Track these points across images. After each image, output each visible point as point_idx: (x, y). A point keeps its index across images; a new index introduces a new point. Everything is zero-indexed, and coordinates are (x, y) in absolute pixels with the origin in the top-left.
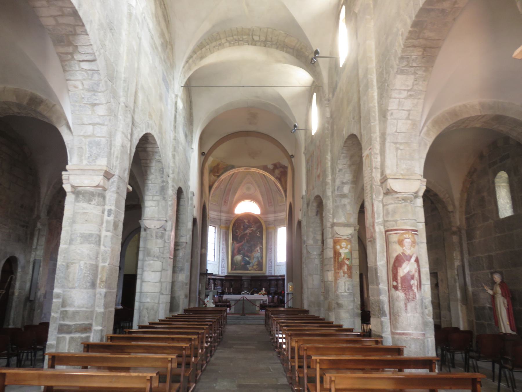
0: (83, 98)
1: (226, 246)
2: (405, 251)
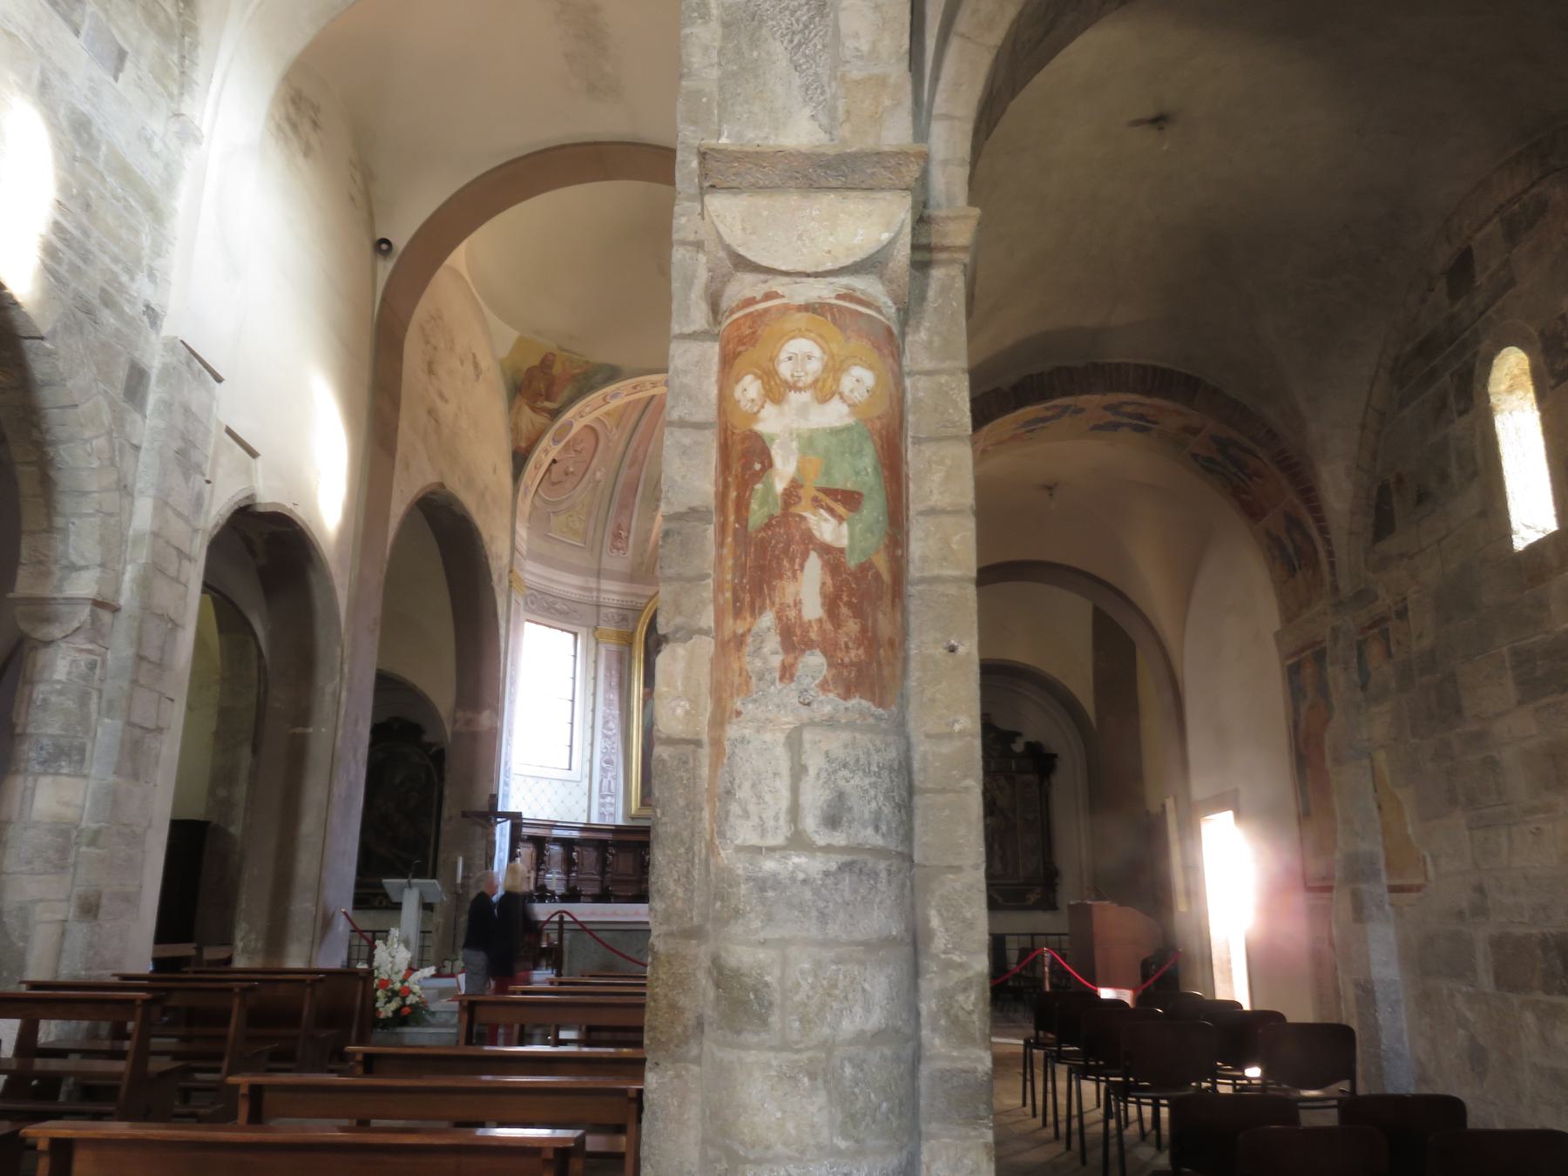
1: (621, 709)
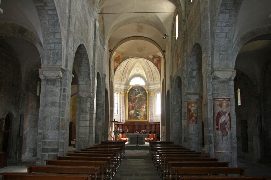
0: (48, 29)
2: (223, 110)
